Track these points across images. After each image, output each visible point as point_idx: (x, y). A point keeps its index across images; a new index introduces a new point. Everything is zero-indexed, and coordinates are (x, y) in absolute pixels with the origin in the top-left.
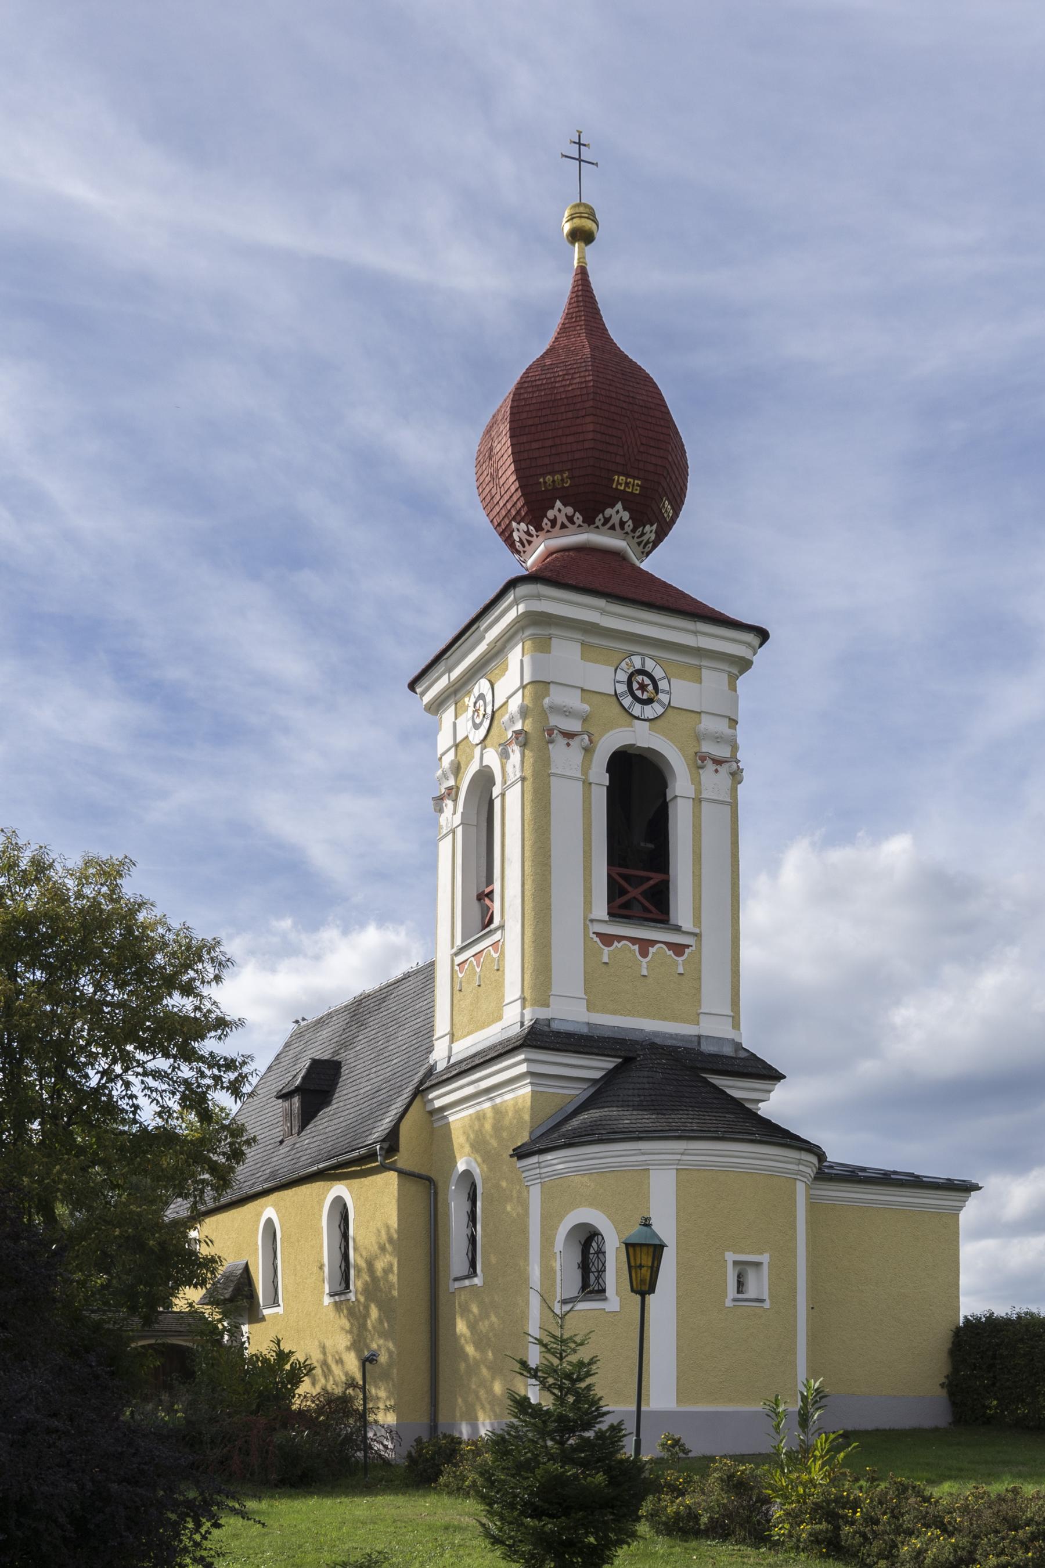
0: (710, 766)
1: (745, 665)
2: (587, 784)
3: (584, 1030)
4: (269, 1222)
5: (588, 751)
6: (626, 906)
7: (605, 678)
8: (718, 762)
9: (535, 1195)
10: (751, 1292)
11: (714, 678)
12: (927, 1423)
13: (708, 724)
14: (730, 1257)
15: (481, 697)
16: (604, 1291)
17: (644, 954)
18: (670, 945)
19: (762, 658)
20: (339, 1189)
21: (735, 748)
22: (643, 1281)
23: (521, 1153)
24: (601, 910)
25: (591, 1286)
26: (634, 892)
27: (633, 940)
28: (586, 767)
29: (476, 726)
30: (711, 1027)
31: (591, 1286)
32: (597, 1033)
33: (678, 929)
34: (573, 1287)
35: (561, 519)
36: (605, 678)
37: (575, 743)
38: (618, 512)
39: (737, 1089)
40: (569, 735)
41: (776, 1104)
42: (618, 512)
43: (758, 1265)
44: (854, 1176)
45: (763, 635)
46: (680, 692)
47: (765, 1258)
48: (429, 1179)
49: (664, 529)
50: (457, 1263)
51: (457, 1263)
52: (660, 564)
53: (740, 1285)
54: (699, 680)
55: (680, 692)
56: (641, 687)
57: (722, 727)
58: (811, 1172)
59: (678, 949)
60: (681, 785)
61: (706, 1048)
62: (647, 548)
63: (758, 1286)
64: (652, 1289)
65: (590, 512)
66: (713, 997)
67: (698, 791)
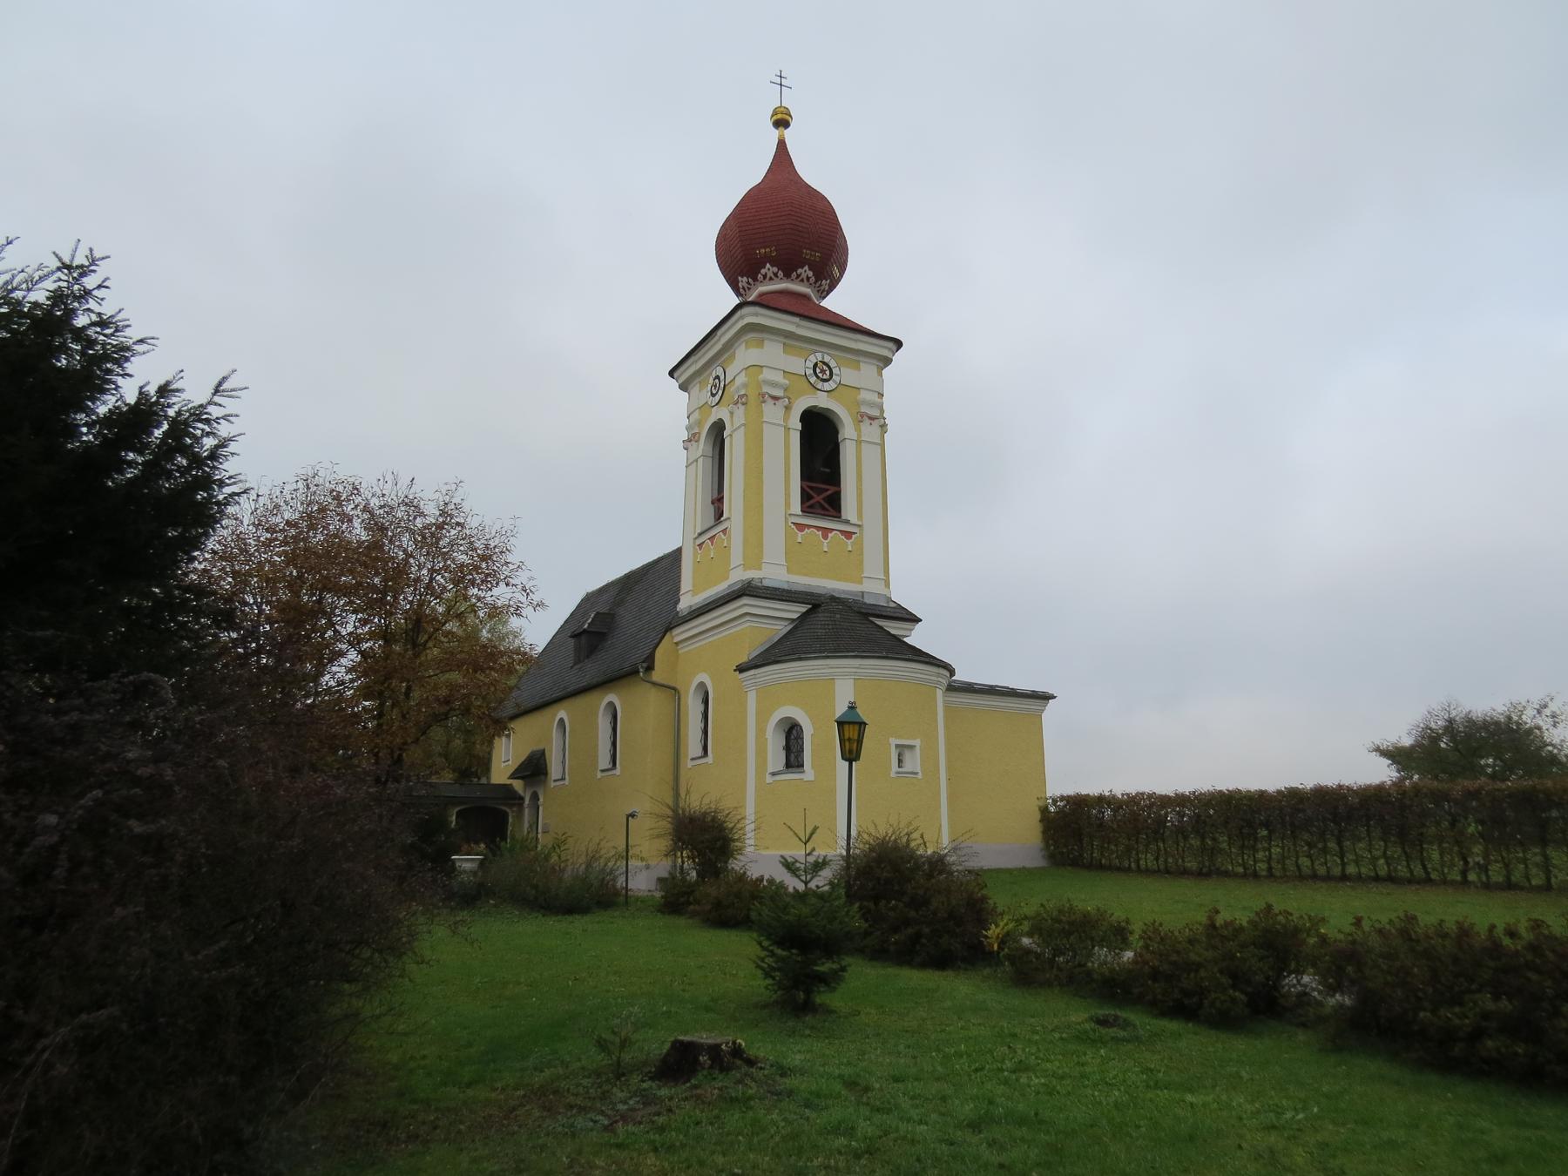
0: (867, 421)
1: (887, 361)
2: (787, 429)
3: (786, 587)
4: (562, 720)
5: (788, 408)
6: (811, 507)
7: (800, 364)
8: (872, 418)
9: (752, 698)
10: (908, 767)
11: (868, 369)
12: (1029, 864)
13: (864, 395)
14: (894, 741)
15: (718, 377)
16: (802, 766)
17: (825, 537)
18: (842, 532)
19: (898, 357)
20: (611, 697)
21: (882, 411)
22: (850, 751)
23: (741, 669)
24: (796, 507)
25: (793, 759)
26: (819, 498)
27: (818, 528)
28: (786, 418)
29: (713, 395)
30: (866, 587)
31: (793, 759)
32: (794, 588)
33: (847, 522)
34: (781, 765)
35: (770, 274)
36: (800, 364)
37: (779, 403)
38: (805, 271)
39: (893, 628)
40: (775, 398)
41: (916, 638)
42: (805, 271)
43: (911, 747)
44: (970, 689)
45: (898, 344)
46: (845, 375)
47: (917, 742)
48: (674, 689)
49: (832, 287)
50: (693, 746)
51: (693, 746)
52: (833, 302)
53: (900, 761)
54: (859, 369)
55: (845, 375)
56: (823, 372)
57: (875, 397)
58: (945, 682)
59: (848, 535)
60: (847, 431)
61: (868, 600)
62: (824, 294)
63: (913, 762)
64: (857, 758)
65: (788, 271)
66: (871, 567)
67: (859, 436)
